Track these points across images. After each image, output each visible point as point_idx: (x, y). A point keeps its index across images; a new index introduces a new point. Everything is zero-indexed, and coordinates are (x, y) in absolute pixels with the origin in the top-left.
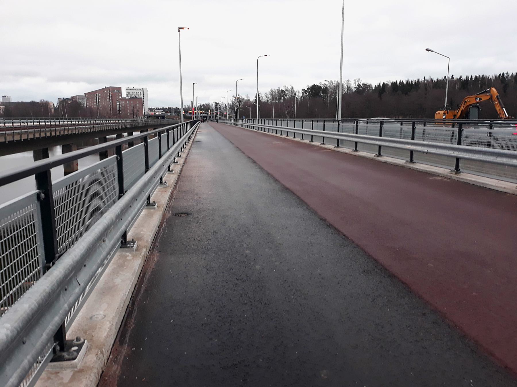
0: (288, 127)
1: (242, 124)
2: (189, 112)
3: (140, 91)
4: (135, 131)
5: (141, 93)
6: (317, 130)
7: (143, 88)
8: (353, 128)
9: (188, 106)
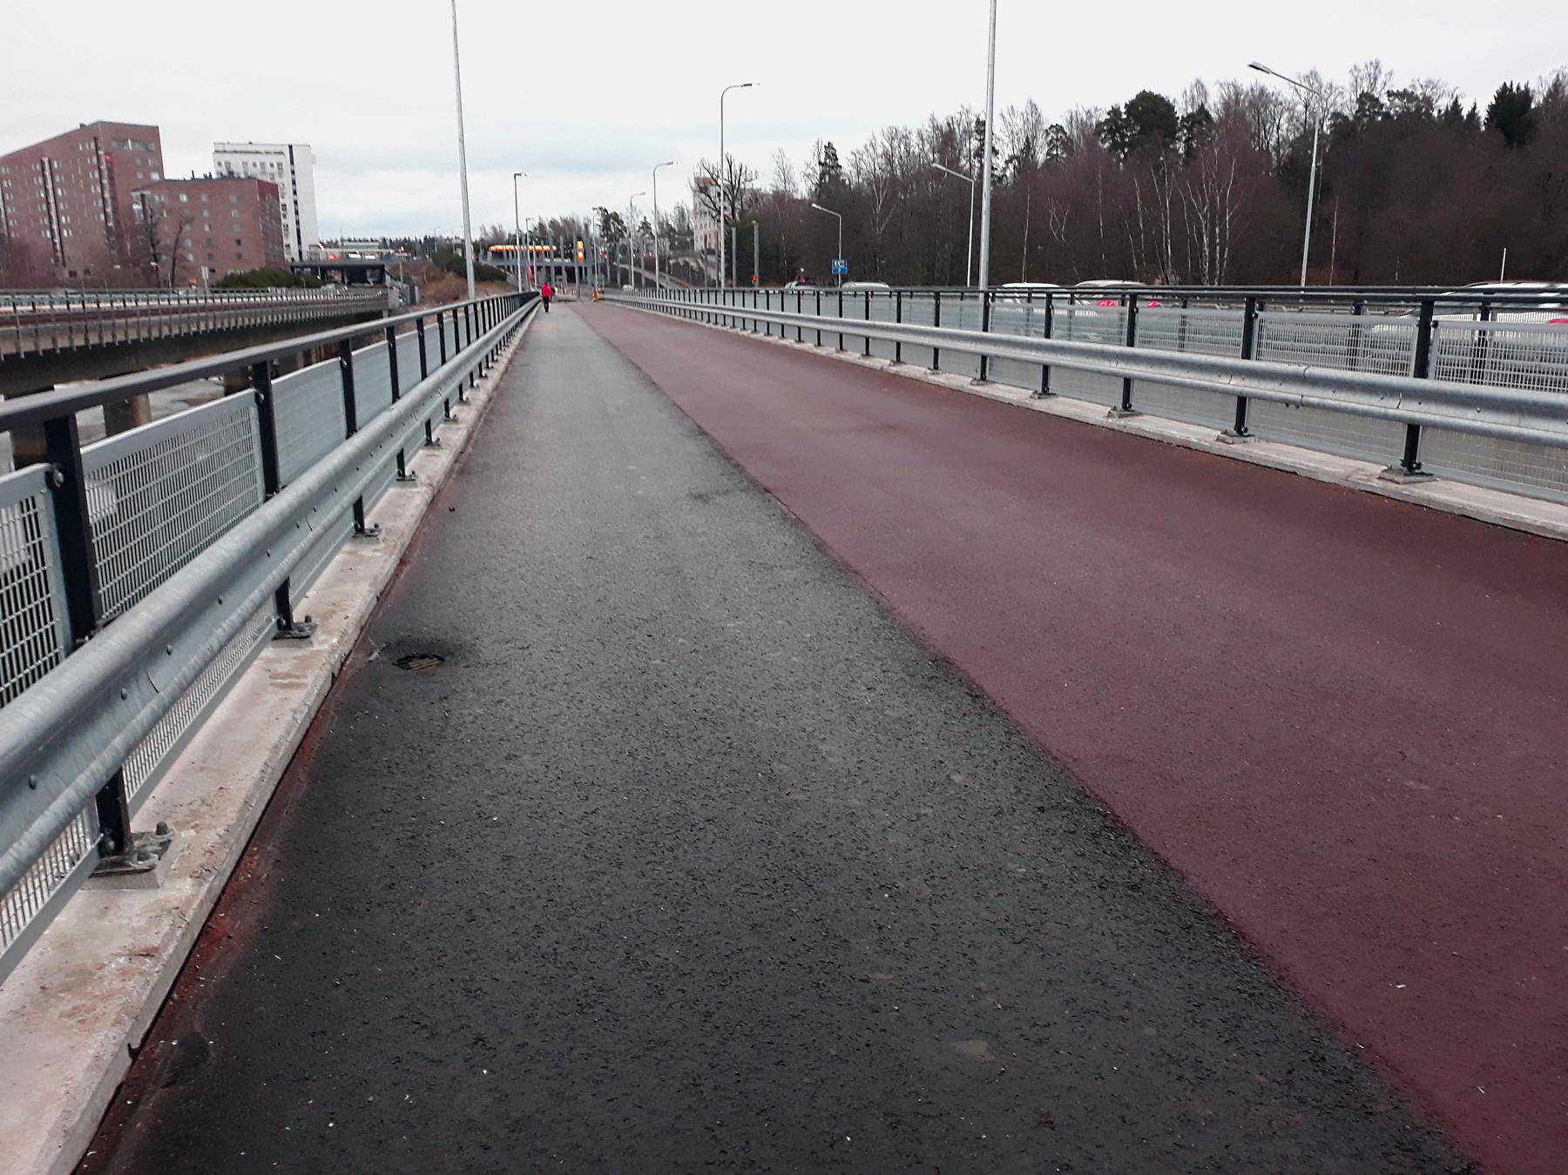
0: (841, 316)
1: (692, 308)
2: (492, 248)
3: (275, 159)
4: (57, 383)
5: (279, 164)
6: (960, 327)
7: (291, 147)
8: (1026, 317)
9: (494, 229)
